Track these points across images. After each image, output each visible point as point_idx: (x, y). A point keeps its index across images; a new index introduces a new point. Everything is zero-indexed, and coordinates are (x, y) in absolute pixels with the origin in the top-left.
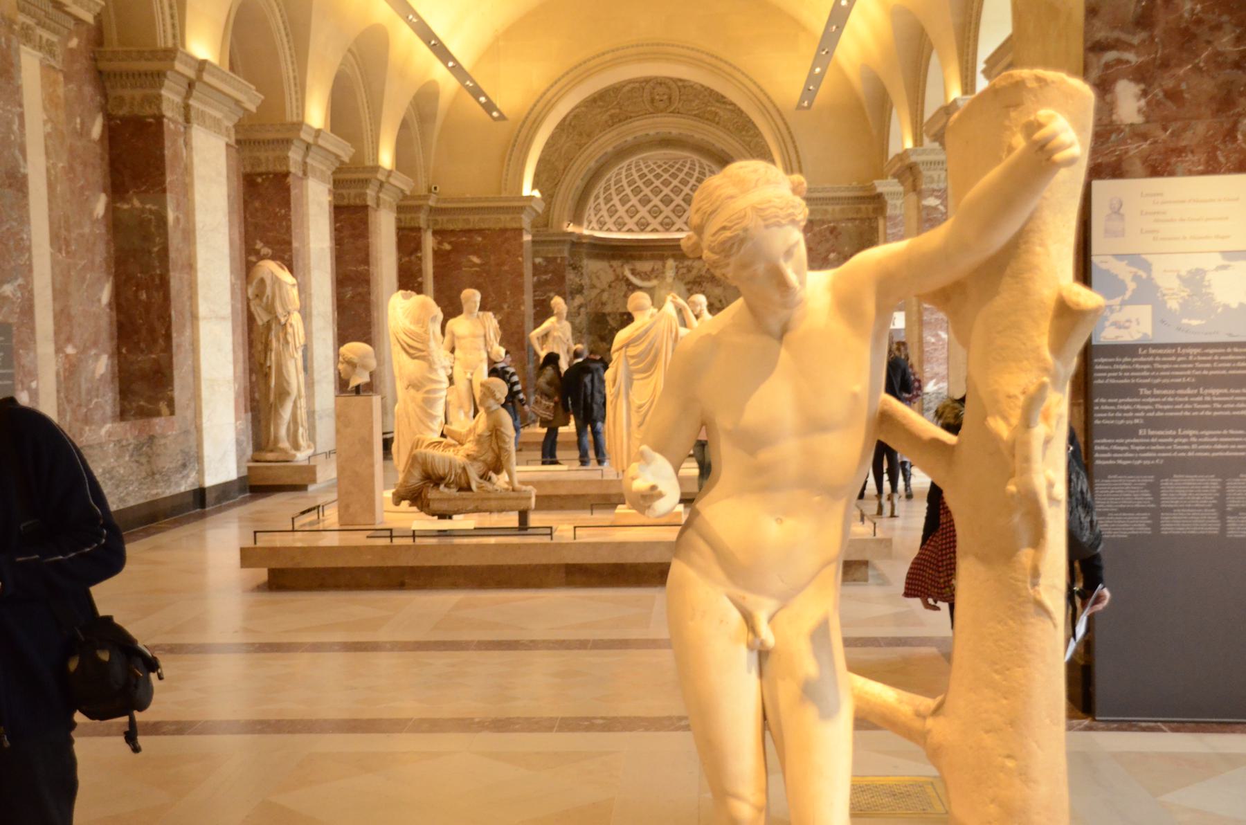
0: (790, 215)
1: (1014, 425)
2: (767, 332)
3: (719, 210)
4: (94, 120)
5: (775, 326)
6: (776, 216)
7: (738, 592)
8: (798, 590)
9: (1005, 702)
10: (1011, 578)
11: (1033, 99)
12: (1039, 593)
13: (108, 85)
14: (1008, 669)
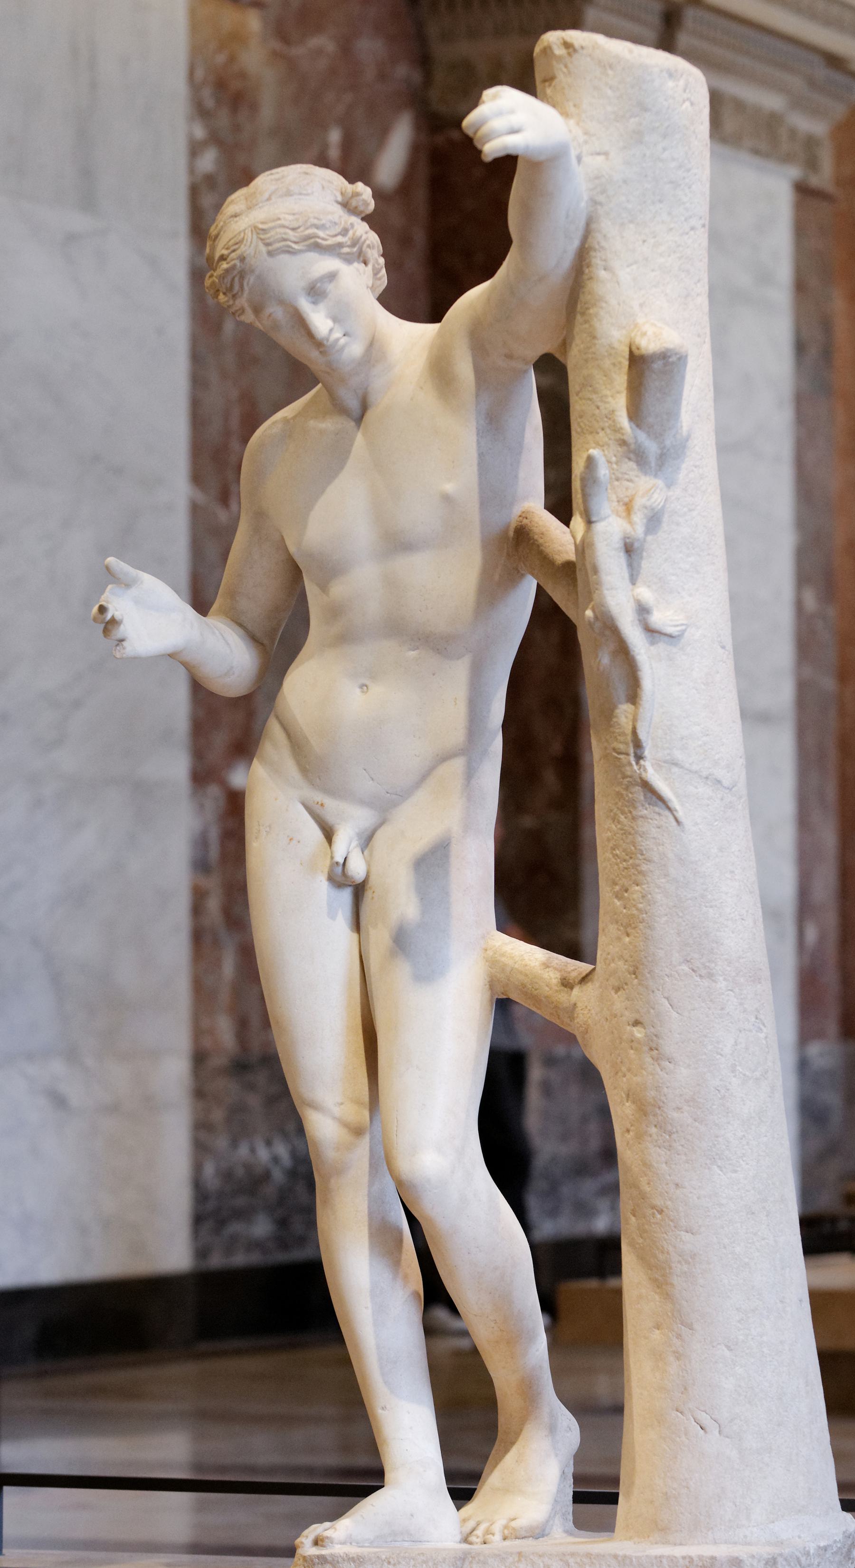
0: (309, 237)
2: (340, 409)
3: (222, 233)
4: (383, 133)
5: (353, 404)
6: (285, 240)
7: (317, 797)
8: (404, 795)
9: (627, 939)
10: (614, 749)
11: (565, 70)
12: (645, 770)
13: (433, 30)
14: (626, 891)
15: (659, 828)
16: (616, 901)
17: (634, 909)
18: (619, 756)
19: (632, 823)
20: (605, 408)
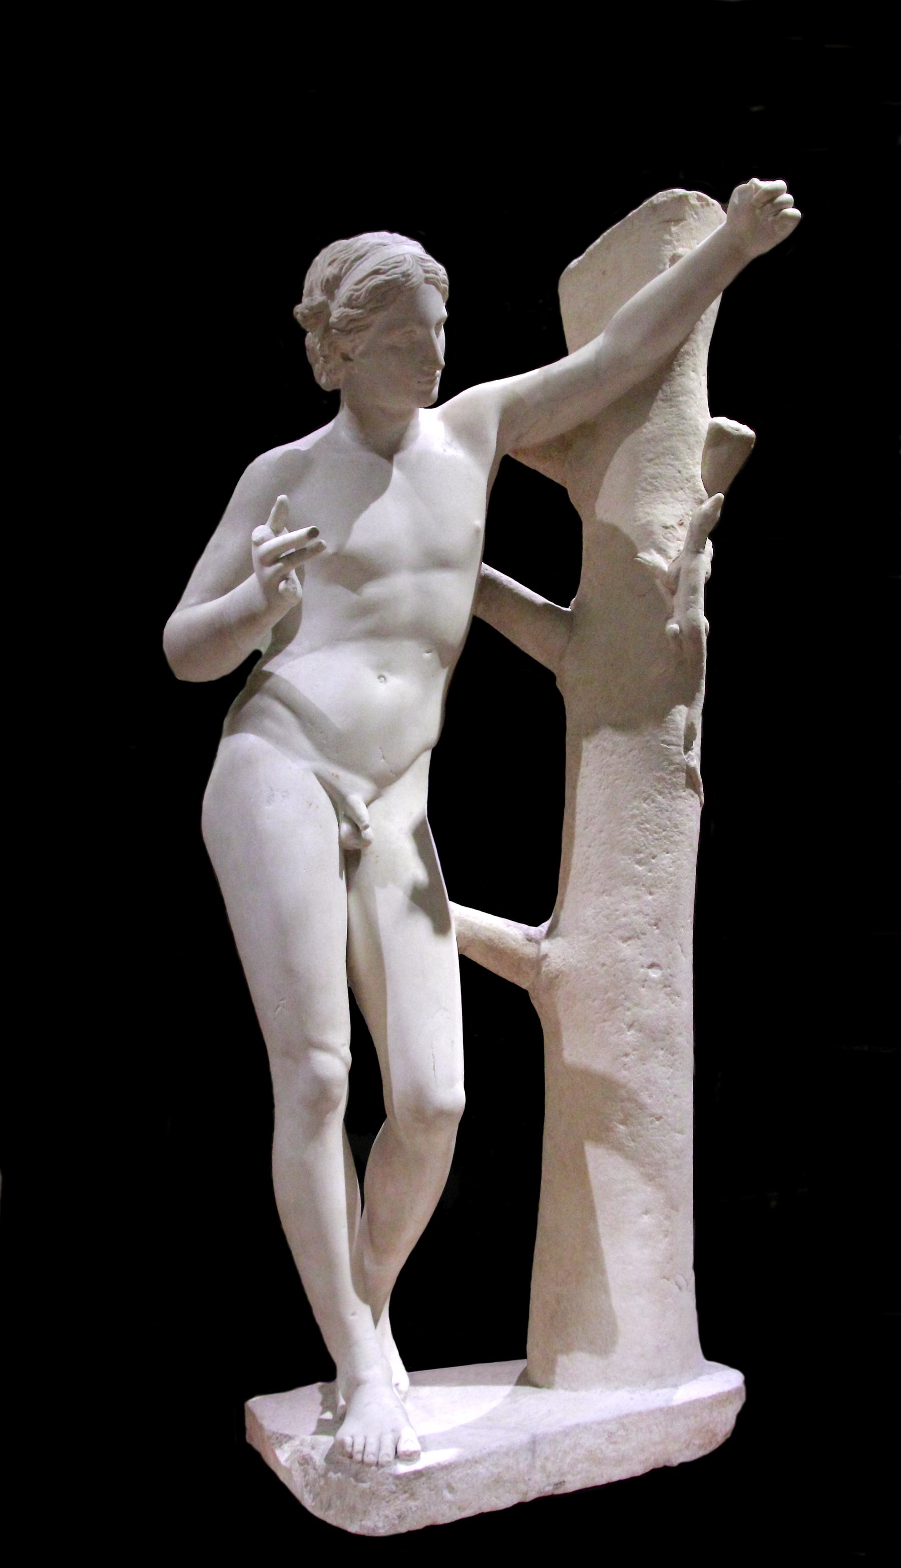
1: (674, 558)
7: (331, 770)
9: (650, 897)
10: (663, 742)
11: (695, 216)
14: (654, 858)
15: (691, 807)
16: (637, 866)
17: (662, 872)
18: (669, 747)
19: (671, 802)
20: (687, 473)
